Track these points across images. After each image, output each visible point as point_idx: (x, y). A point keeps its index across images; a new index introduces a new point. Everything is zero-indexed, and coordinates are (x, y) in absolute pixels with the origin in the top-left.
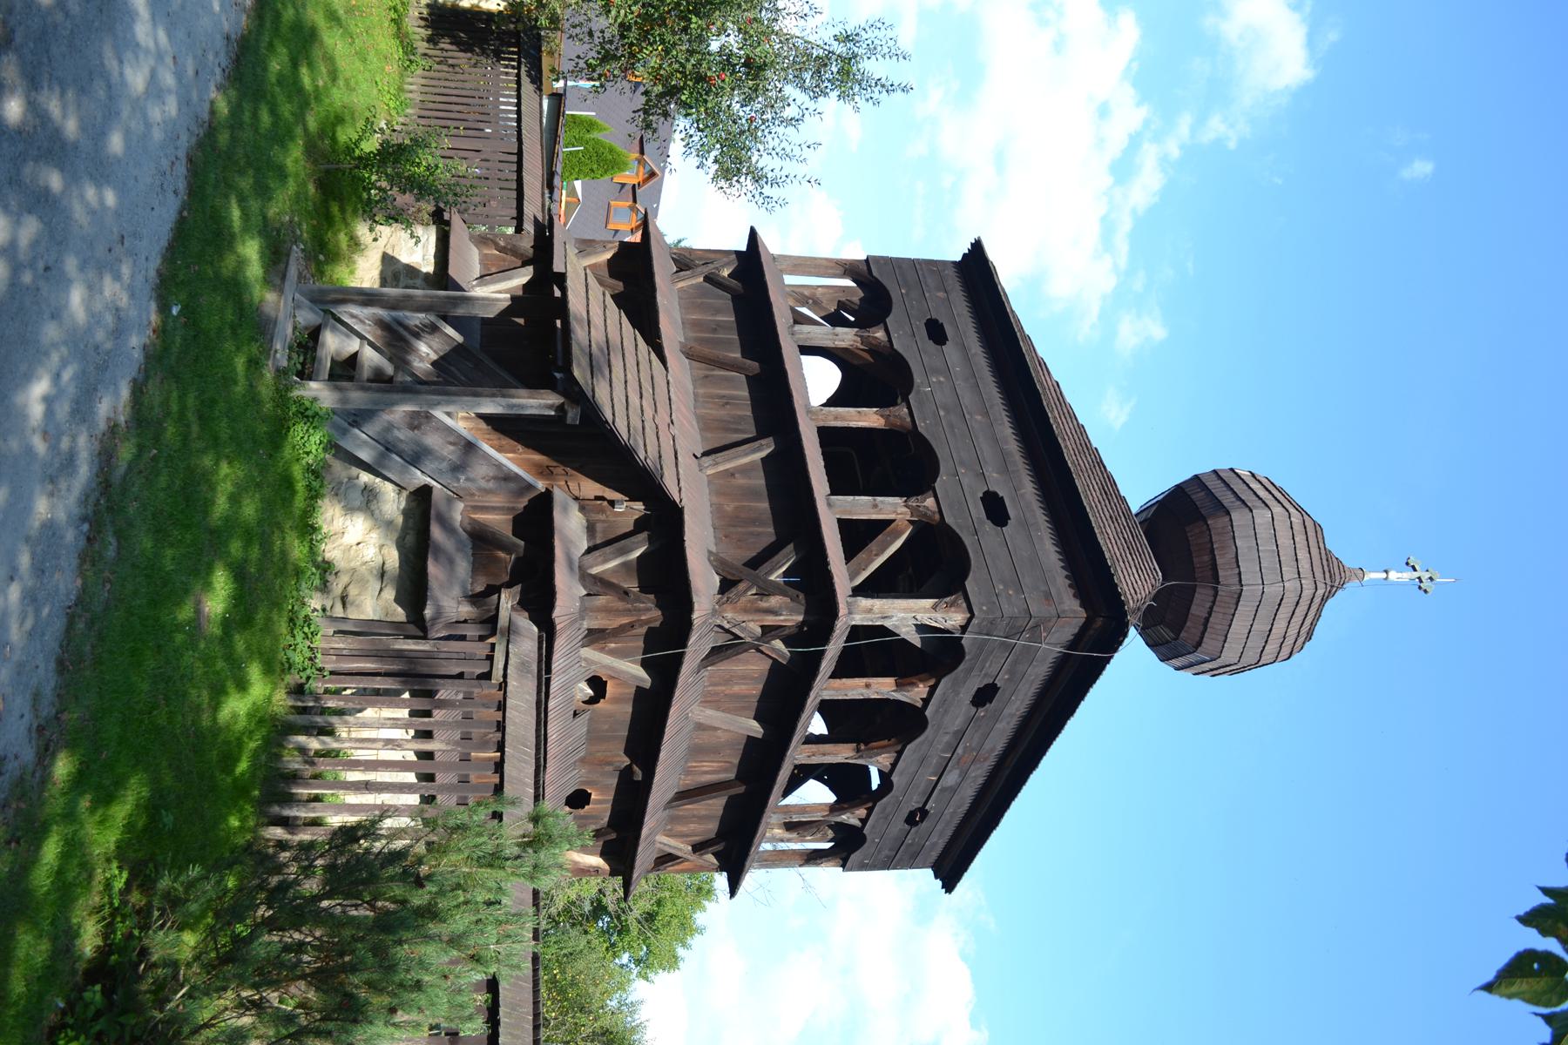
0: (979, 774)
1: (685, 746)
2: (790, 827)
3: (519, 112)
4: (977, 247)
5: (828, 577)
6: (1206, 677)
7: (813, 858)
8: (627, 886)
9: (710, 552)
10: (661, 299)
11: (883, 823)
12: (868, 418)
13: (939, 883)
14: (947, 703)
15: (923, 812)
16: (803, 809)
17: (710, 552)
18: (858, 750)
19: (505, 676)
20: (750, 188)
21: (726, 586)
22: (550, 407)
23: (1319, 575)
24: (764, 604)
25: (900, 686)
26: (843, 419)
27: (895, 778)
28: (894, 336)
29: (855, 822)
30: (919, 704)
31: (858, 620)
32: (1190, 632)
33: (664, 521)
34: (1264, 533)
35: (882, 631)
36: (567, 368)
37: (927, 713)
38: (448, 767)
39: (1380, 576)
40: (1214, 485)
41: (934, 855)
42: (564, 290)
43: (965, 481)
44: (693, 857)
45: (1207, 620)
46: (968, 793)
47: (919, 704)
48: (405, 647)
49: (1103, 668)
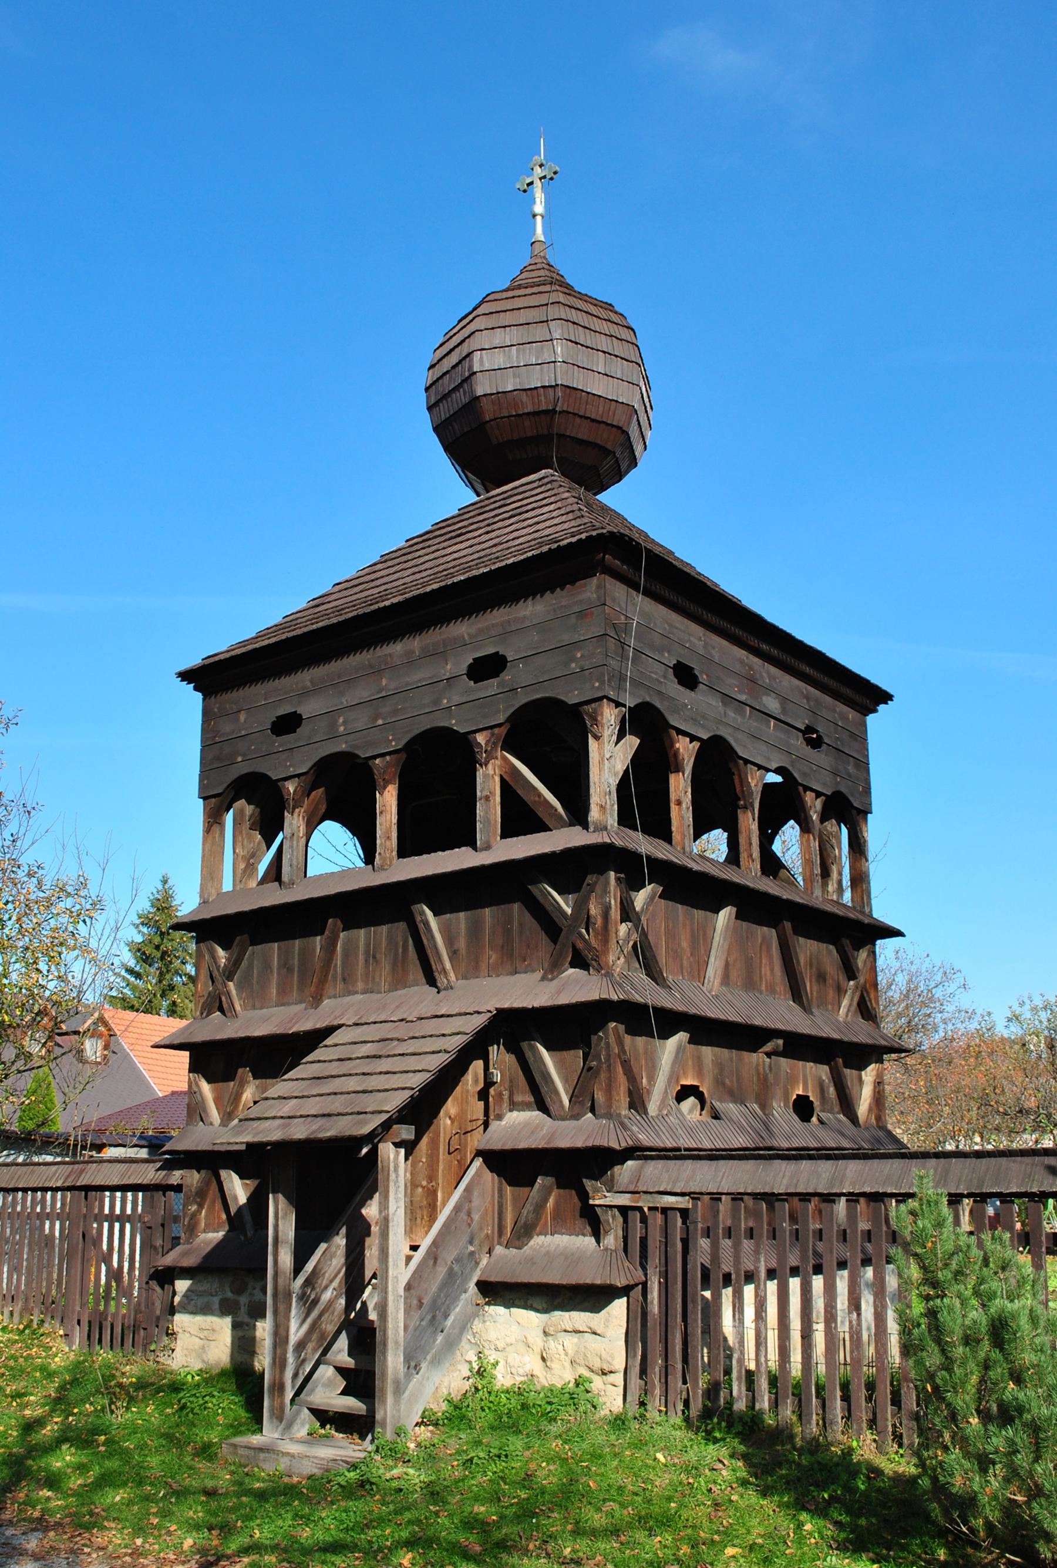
0: (766, 672)
2: (826, 874)
3: (35, 1190)
4: (186, 676)
5: (569, 853)
7: (858, 847)
9: (543, 979)
11: (818, 773)
13: (881, 707)
14: (694, 716)
16: (807, 863)
17: (543, 979)
18: (745, 807)
19: (683, 1194)
21: (580, 962)
24: (599, 921)
25: (678, 769)
26: (389, 830)
28: (292, 771)
29: (819, 804)
30: (696, 745)
31: (612, 819)
32: (602, 437)
33: (511, 1028)
35: (623, 786)
37: (705, 738)
40: (445, 411)
41: (852, 714)
43: (456, 699)
45: (593, 420)
46: (787, 682)
47: (696, 745)
48: (656, 1302)
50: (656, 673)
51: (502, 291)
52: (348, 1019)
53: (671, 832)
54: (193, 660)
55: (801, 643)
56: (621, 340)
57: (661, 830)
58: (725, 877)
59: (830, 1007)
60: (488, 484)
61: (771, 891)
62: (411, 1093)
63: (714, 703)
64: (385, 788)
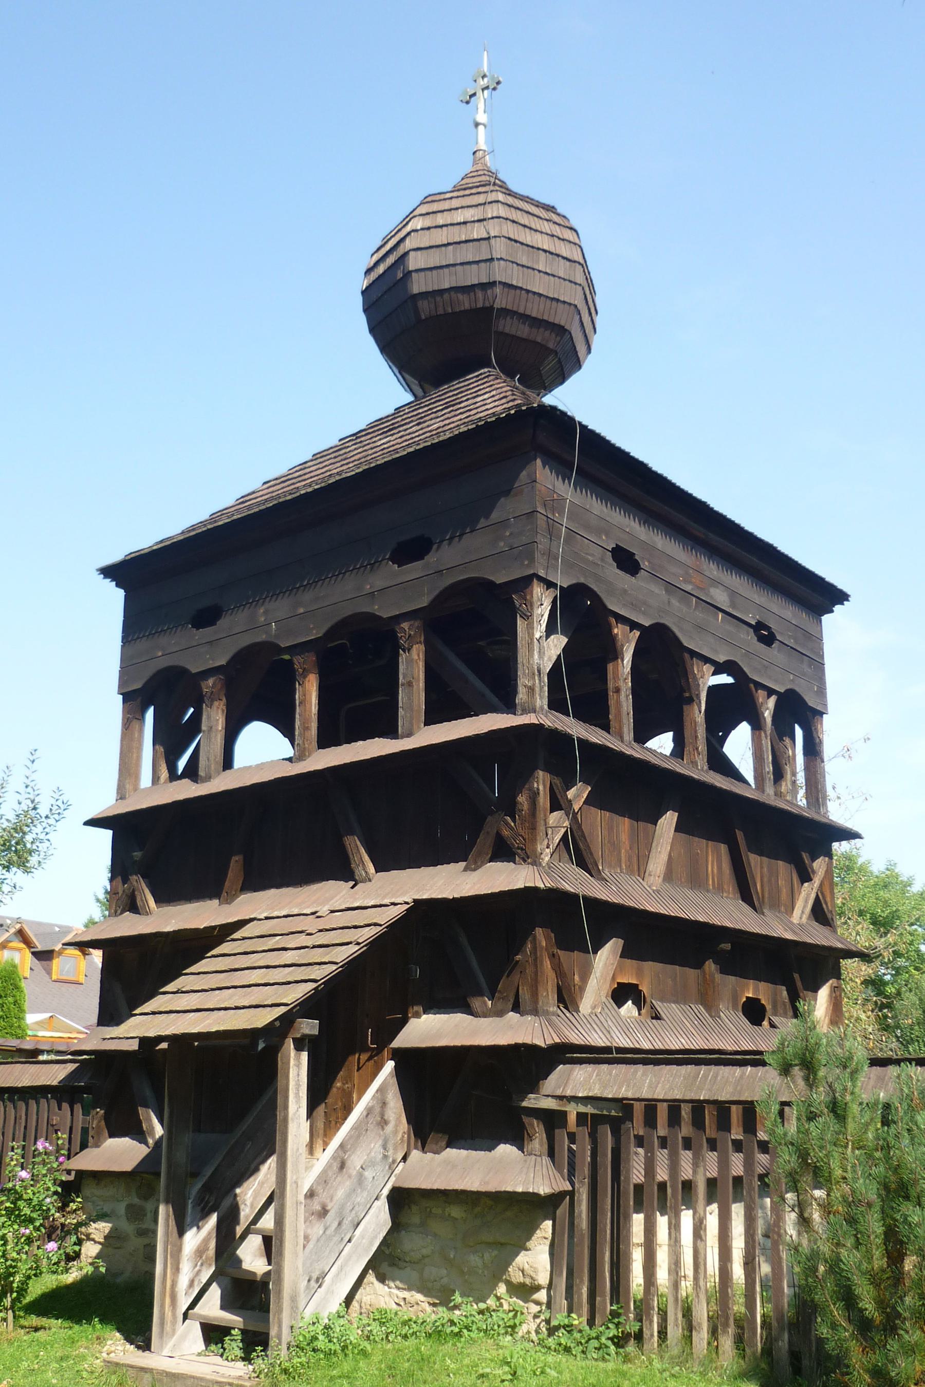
1: (690, 893)
2: (779, 775)
4: (108, 572)
6: (598, 320)
7: (813, 749)
8: (850, 954)
9: (465, 869)
10: (169, 927)
11: (772, 671)
12: (309, 694)
13: (837, 608)
14: (635, 601)
15: (759, 627)
17: (465, 869)
20: (39, 829)
22: (298, 1058)
23: (481, 199)
27: (721, 659)
29: (772, 702)
31: (542, 700)
34: (434, 259)
36: (253, 1034)
38: (724, 1164)
39: (486, 134)
42: (160, 1039)
44: (816, 882)
49: (592, 432)
50: (593, 555)
52: (261, 913)
54: (116, 555)
55: (750, 535)
56: (563, 240)
57: (594, 709)
58: (667, 766)
59: (783, 909)
60: (426, 386)
61: (718, 785)
62: (314, 985)
63: (657, 591)
64: (305, 677)
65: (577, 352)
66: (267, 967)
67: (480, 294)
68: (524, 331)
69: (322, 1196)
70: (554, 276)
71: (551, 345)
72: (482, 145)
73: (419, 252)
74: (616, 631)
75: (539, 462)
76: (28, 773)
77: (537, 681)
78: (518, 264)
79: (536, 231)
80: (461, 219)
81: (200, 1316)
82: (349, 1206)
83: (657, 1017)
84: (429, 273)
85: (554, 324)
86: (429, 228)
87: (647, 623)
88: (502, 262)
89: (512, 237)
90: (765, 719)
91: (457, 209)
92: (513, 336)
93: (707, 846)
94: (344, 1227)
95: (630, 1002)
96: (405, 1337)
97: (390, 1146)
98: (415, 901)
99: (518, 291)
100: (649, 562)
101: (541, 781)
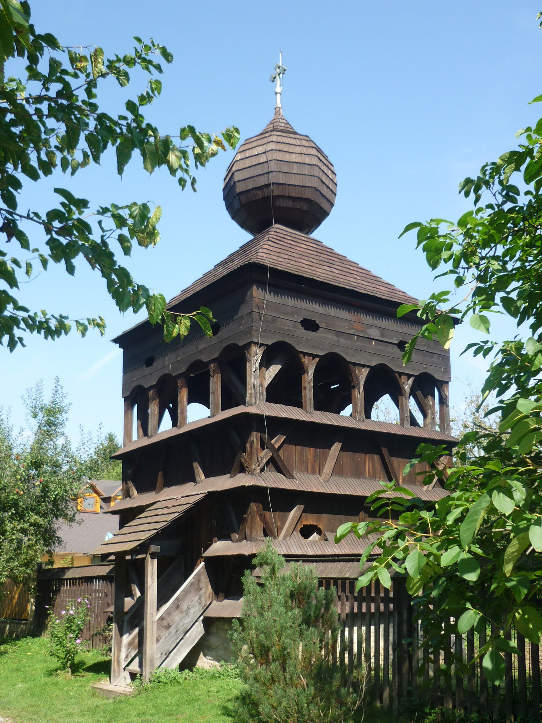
4: (116, 341)
7: (443, 401)
11: (406, 367)
22: (152, 562)
23: (265, 141)
39: (280, 99)
51: (258, 136)
53: (302, 403)
65: (323, 208)
66: (148, 523)
67: (266, 190)
68: (290, 204)
69: (168, 620)
70: (302, 174)
71: (305, 208)
72: (279, 105)
73: (239, 172)
74: (303, 360)
75: (255, 287)
76: (99, 434)
77: (253, 391)
78: (283, 172)
79: (292, 153)
80: (256, 153)
81: (130, 670)
82: (181, 624)
83: (326, 540)
84: (243, 182)
85: (305, 198)
86: (242, 159)
87: (322, 354)
88: (274, 173)
89: (279, 159)
90: (405, 390)
91: (255, 147)
92: (285, 207)
93: (365, 457)
94: (179, 632)
95: (315, 533)
96: (202, 678)
97: (203, 599)
98: (208, 492)
99: (284, 186)
100: (325, 323)
101: (255, 437)
